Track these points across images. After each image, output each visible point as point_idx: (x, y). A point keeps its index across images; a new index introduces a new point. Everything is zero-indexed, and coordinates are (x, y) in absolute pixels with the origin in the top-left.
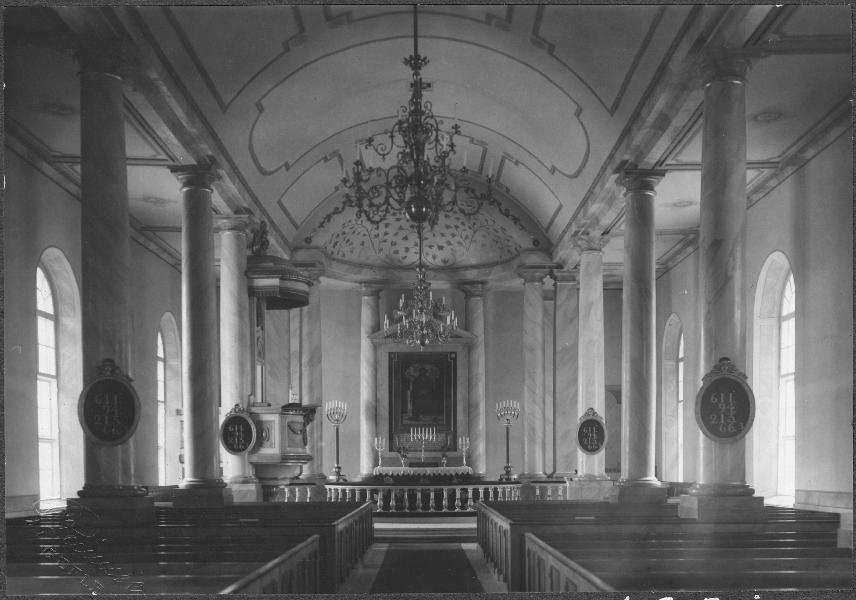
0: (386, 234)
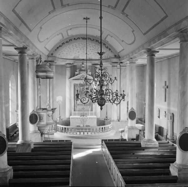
0: (73, 51)
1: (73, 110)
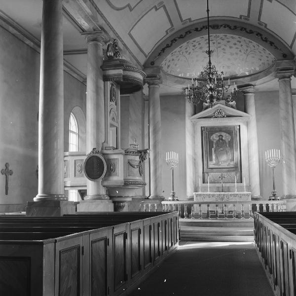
1: (200, 180)
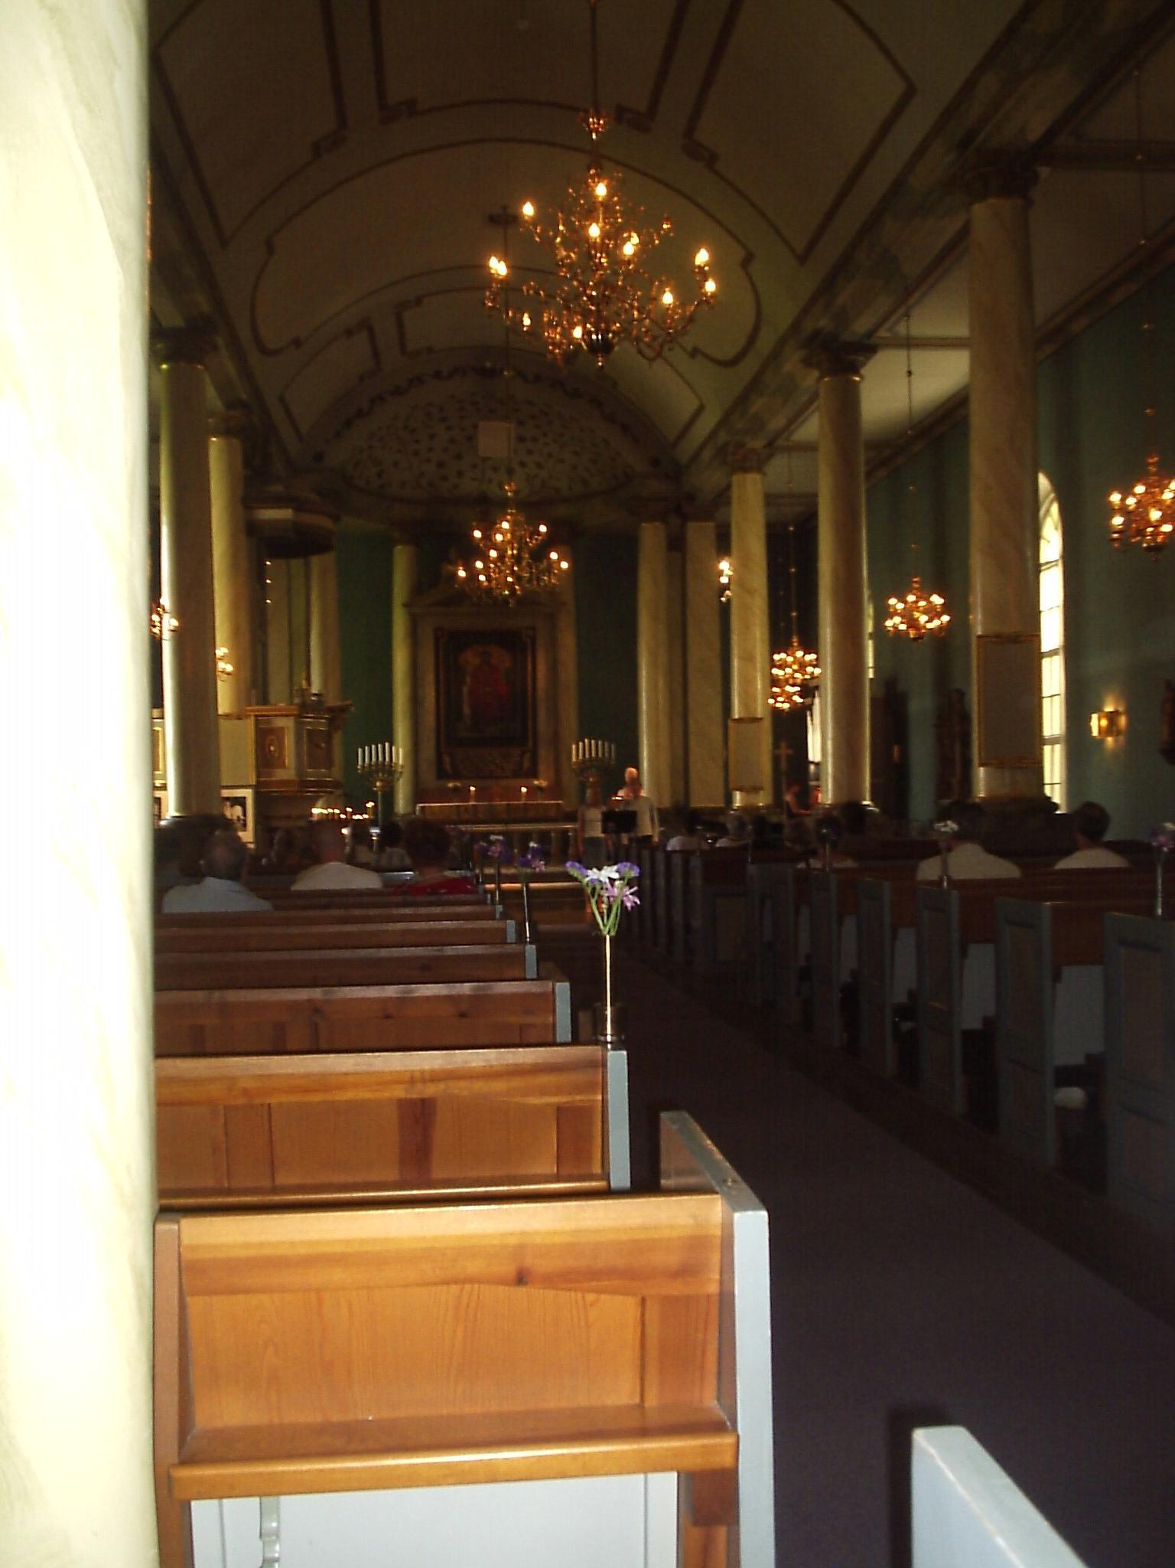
0: (431, 449)
